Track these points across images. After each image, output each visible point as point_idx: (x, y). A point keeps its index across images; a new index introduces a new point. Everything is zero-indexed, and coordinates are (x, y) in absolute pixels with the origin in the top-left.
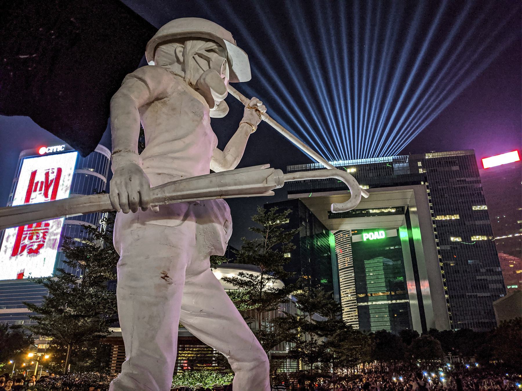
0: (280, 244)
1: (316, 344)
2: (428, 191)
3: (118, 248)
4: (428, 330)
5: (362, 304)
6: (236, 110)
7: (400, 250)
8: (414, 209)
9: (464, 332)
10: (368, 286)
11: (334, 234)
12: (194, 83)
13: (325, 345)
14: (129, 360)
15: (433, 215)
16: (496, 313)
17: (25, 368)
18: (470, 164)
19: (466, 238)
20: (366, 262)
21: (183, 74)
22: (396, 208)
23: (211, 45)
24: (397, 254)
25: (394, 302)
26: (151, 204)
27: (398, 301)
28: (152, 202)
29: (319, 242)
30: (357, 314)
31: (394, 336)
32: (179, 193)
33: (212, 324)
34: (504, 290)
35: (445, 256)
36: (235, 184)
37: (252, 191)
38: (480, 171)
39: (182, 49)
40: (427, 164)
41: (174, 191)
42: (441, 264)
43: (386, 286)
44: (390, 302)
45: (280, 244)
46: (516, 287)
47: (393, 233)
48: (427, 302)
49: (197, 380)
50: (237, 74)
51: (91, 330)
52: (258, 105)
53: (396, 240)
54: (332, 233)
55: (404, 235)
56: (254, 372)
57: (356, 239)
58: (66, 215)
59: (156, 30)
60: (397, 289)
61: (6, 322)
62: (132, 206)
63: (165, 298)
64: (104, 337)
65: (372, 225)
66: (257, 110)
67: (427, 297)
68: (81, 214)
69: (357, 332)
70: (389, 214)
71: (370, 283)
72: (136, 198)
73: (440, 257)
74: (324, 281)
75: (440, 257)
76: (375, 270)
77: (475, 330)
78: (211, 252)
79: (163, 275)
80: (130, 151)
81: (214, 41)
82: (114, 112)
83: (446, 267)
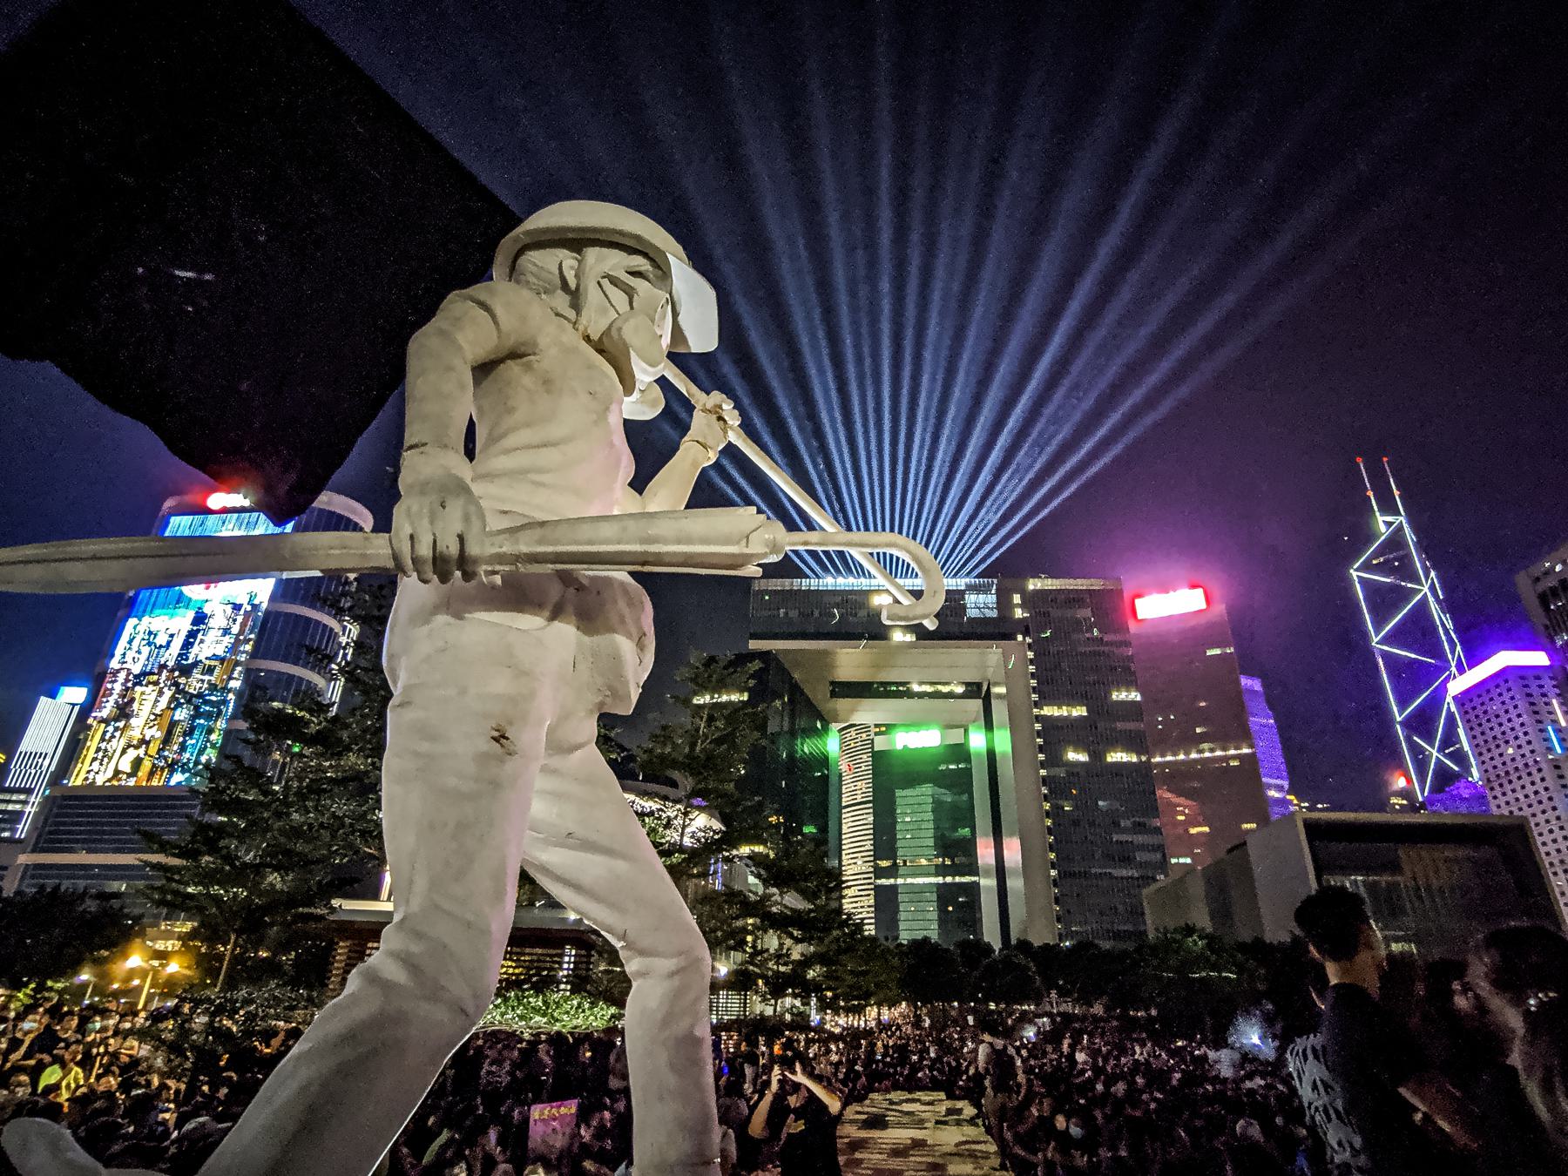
0: (732, 734)
1: (788, 956)
2: (1030, 655)
3: (393, 671)
4: (1014, 941)
5: (883, 881)
6: (677, 414)
7: (967, 773)
8: (1002, 690)
9: (1084, 946)
10: (899, 844)
11: (840, 730)
12: (595, 337)
13: (807, 962)
14: (402, 921)
15: (1036, 704)
16: (1147, 911)
17: (116, 995)
18: (1111, 608)
19: (1097, 756)
20: (899, 793)
21: (571, 314)
22: (967, 684)
23: (639, 262)
24: (961, 782)
25: (949, 879)
26: (484, 567)
27: (958, 879)
28: (487, 563)
29: (807, 747)
30: (872, 902)
31: (947, 950)
32: (550, 549)
33: (591, 867)
34: (1164, 865)
35: (1056, 788)
36: (679, 542)
37: (715, 561)
38: (1133, 627)
39: (575, 264)
40: (1031, 600)
41: (540, 542)
42: (1047, 806)
43: (936, 846)
44: (940, 880)
45: (732, 734)
46: (1188, 861)
47: (956, 737)
48: (1015, 884)
49: (536, 1010)
50: (687, 334)
51: (289, 900)
52: (725, 407)
53: (959, 752)
54: (835, 727)
55: (977, 741)
56: (676, 981)
57: (880, 744)
58: (282, 570)
59: (520, 221)
60: (955, 850)
61: (82, 883)
62: (441, 566)
63: (495, 785)
64: (321, 918)
65: (915, 722)
66: (720, 418)
67: (1014, 872)
68: (318, 574)
69: (873, 939)
70: (951, 695)
71: (904, 837)
72: (453, 550)
73: (1045, 791)
74: (809, 829)
75: (1045, 791)
76: (916, 811)
77: (1106, 945)
78: (602, 704)
79: (496, 734)
80: (446, 446)
81: (645, 255)
82: (413, 364)
83: (1055, 813)
